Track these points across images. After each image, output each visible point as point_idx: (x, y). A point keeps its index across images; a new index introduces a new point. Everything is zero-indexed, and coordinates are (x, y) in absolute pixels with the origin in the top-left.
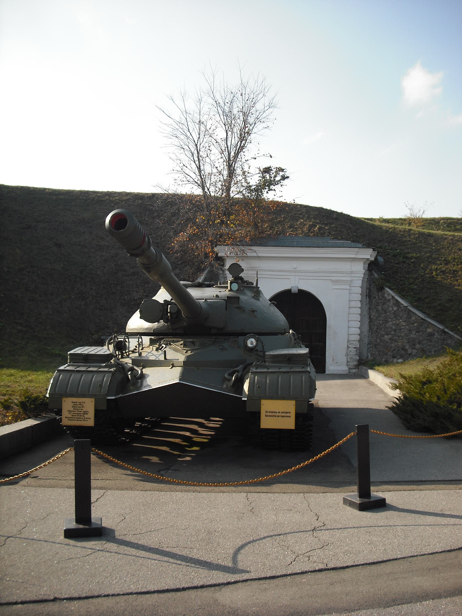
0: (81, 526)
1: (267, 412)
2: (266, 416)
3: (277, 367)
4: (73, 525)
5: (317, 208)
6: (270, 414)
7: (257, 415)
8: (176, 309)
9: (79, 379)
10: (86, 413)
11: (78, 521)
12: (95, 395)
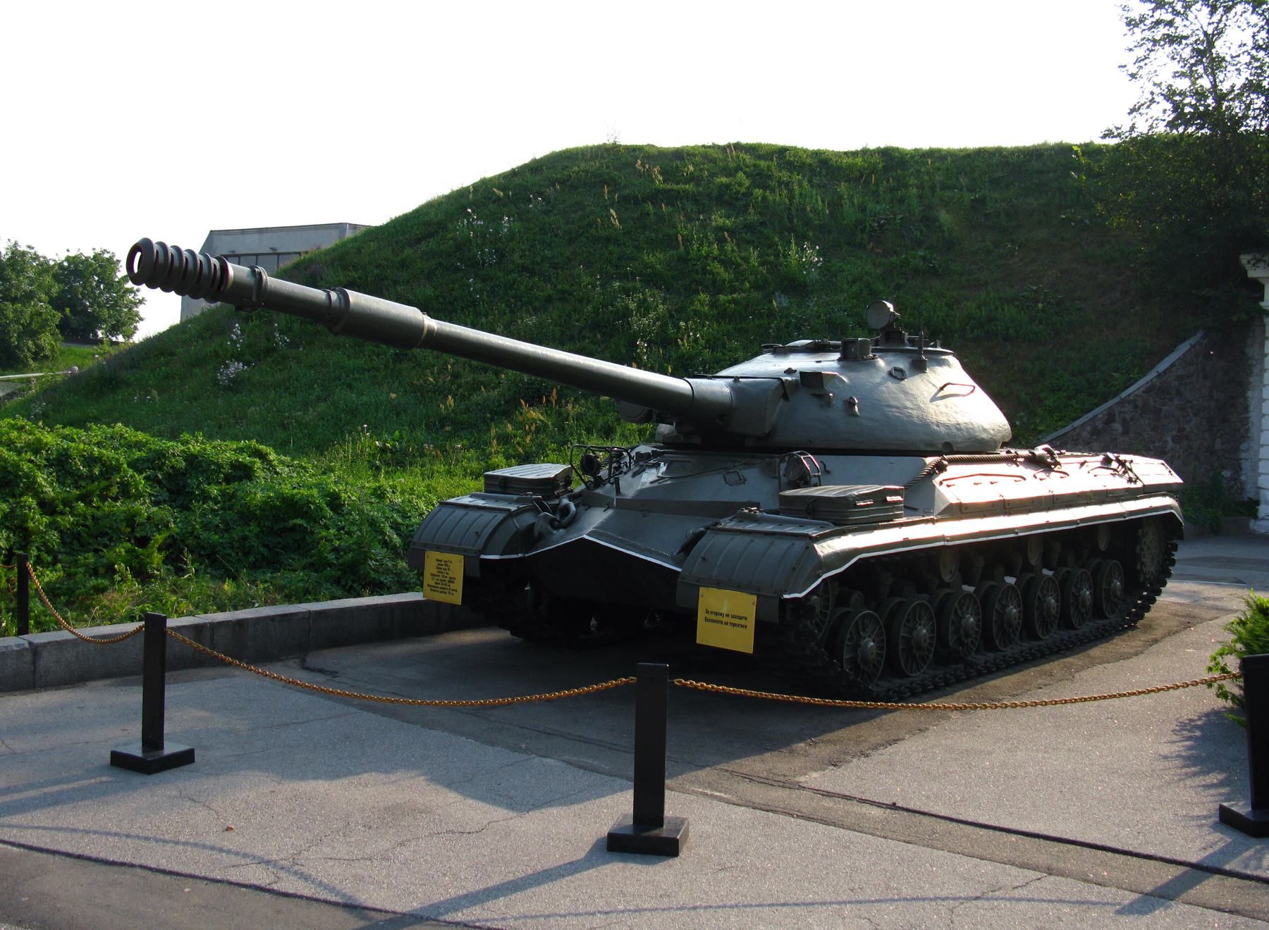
1: (707, 612)
2: (706, 620)
3: (504, 500)
6: (713, 617)
7: (688, 620)
12: (466, 551)
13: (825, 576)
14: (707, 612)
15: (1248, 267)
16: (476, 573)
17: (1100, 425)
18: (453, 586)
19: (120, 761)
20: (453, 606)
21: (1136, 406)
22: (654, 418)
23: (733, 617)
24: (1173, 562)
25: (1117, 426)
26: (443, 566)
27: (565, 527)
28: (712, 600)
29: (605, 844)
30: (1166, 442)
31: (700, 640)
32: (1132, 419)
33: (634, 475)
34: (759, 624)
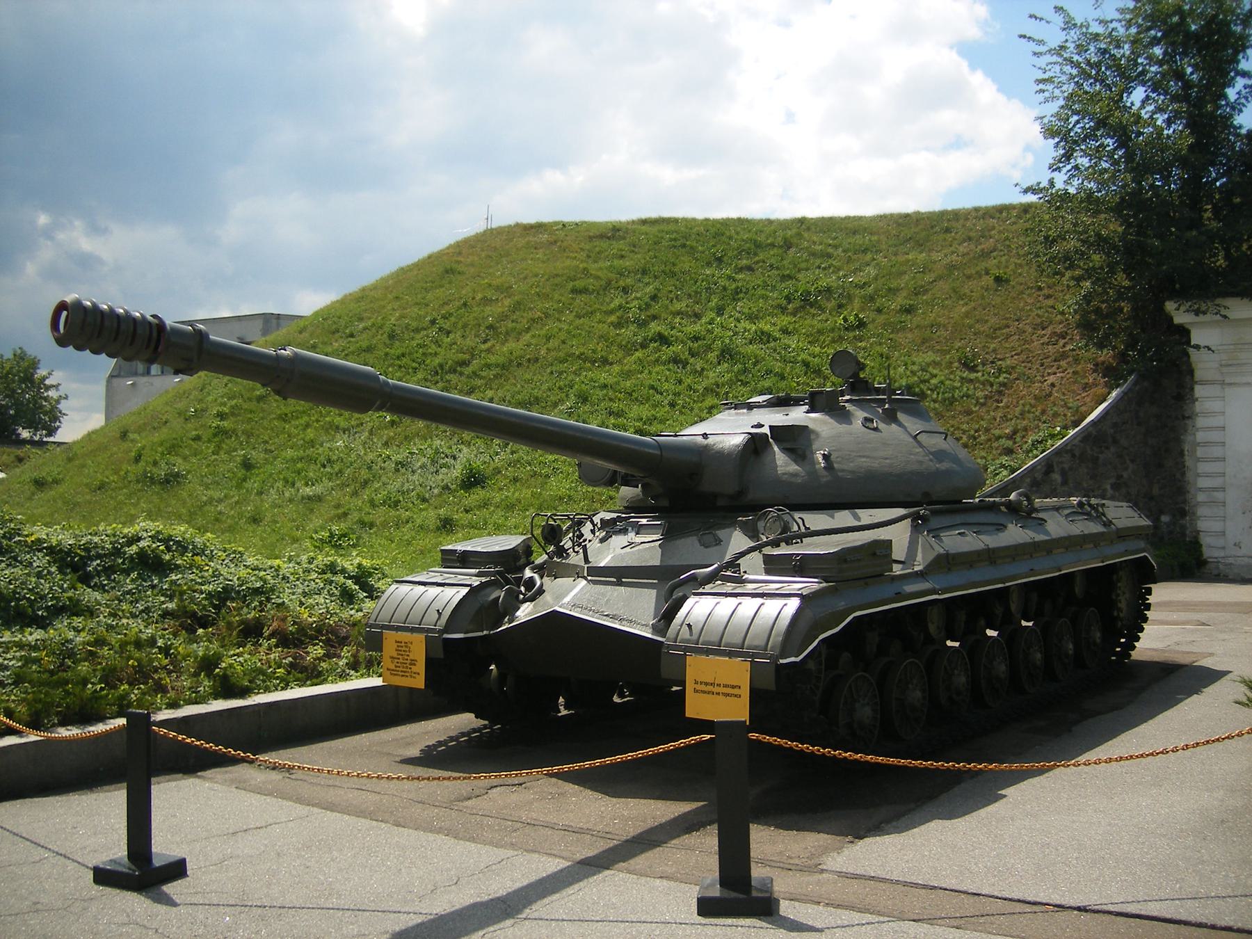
0: (733, 895)
1: (696, 683)
2: (696, 691)
4: (716, 892)
5: (907, 216)
6: (703, 687)
8: (1211, 548)
9: (766, 635)
10: (413, 662)
11: (724, 881)
13: (821, 637)
14: (696, 683)
15: (1173, 313)
16: (440, 654)
17: (1038, 476)
18: (414, 669)
19: (104, 877)
20: (412, 690)
21: (1073, 456)
22: (619, 480)
23: (725, 686)
24: (1148, 607)
25: (1056, 477)
26: (402, 647)
27: (532, 600)
28: (697, 669)
29: (769, 919)
30: (1105, 490)
31: (689, 713)
32: (1071, 469)
33: (602, 540)
34: (753, 691)
